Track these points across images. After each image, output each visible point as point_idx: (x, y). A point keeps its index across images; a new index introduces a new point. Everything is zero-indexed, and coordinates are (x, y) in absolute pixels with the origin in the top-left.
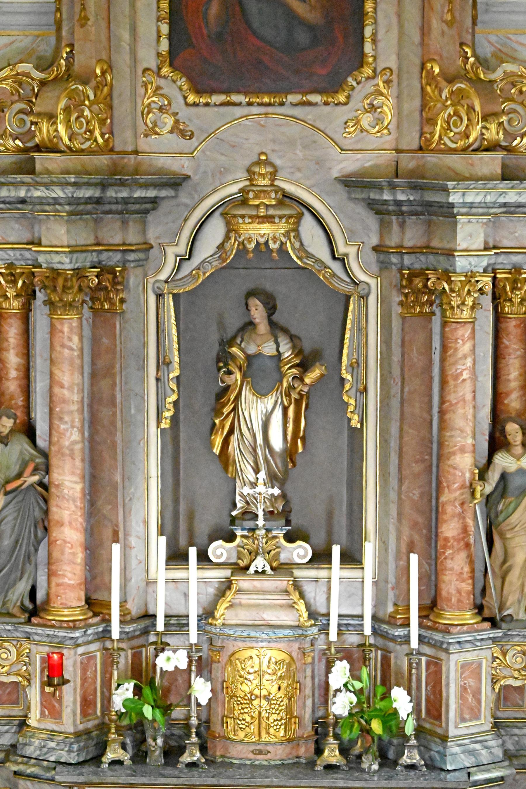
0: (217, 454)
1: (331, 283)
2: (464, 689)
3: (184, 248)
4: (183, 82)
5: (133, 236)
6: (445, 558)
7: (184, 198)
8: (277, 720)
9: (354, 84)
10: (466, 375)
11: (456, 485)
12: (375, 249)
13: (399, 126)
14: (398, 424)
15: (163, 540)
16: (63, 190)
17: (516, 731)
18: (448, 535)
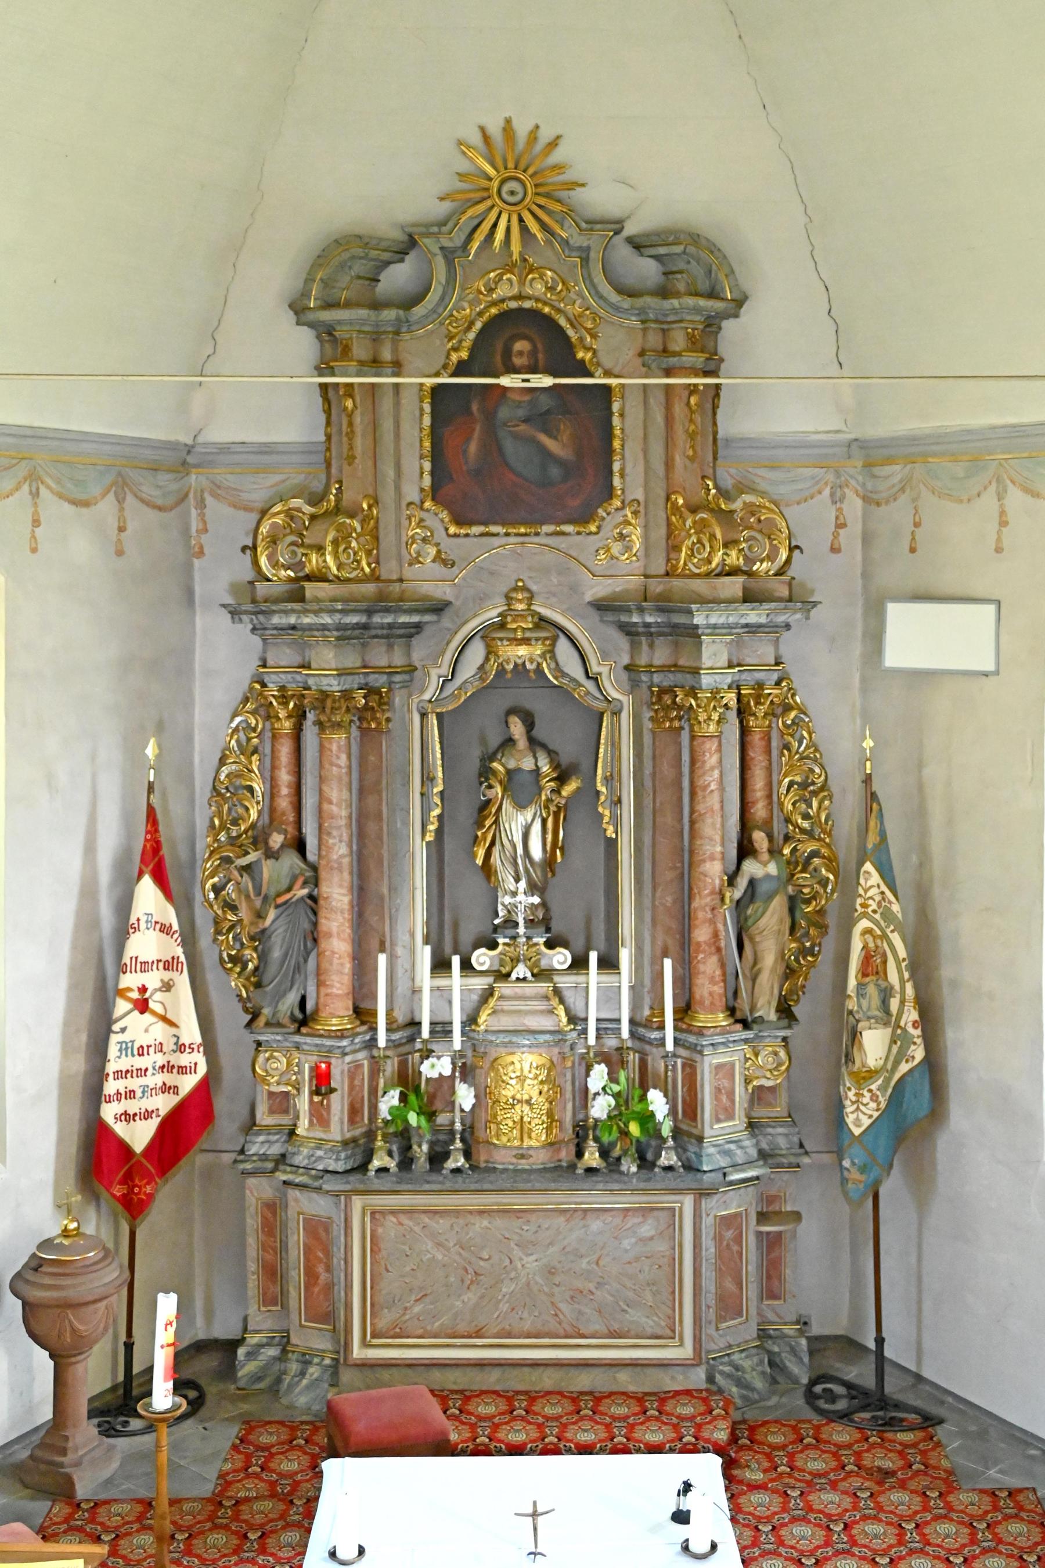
2: (718, 1090)
3: (445, 671)
4: (444, 515)
5: (398, 659)
6: (698, 962)
7: (446, 621)
9: (604, 514)
10: (713, 786)
13: (647, 555)
15: (428, 949)
17: (770, 1130)
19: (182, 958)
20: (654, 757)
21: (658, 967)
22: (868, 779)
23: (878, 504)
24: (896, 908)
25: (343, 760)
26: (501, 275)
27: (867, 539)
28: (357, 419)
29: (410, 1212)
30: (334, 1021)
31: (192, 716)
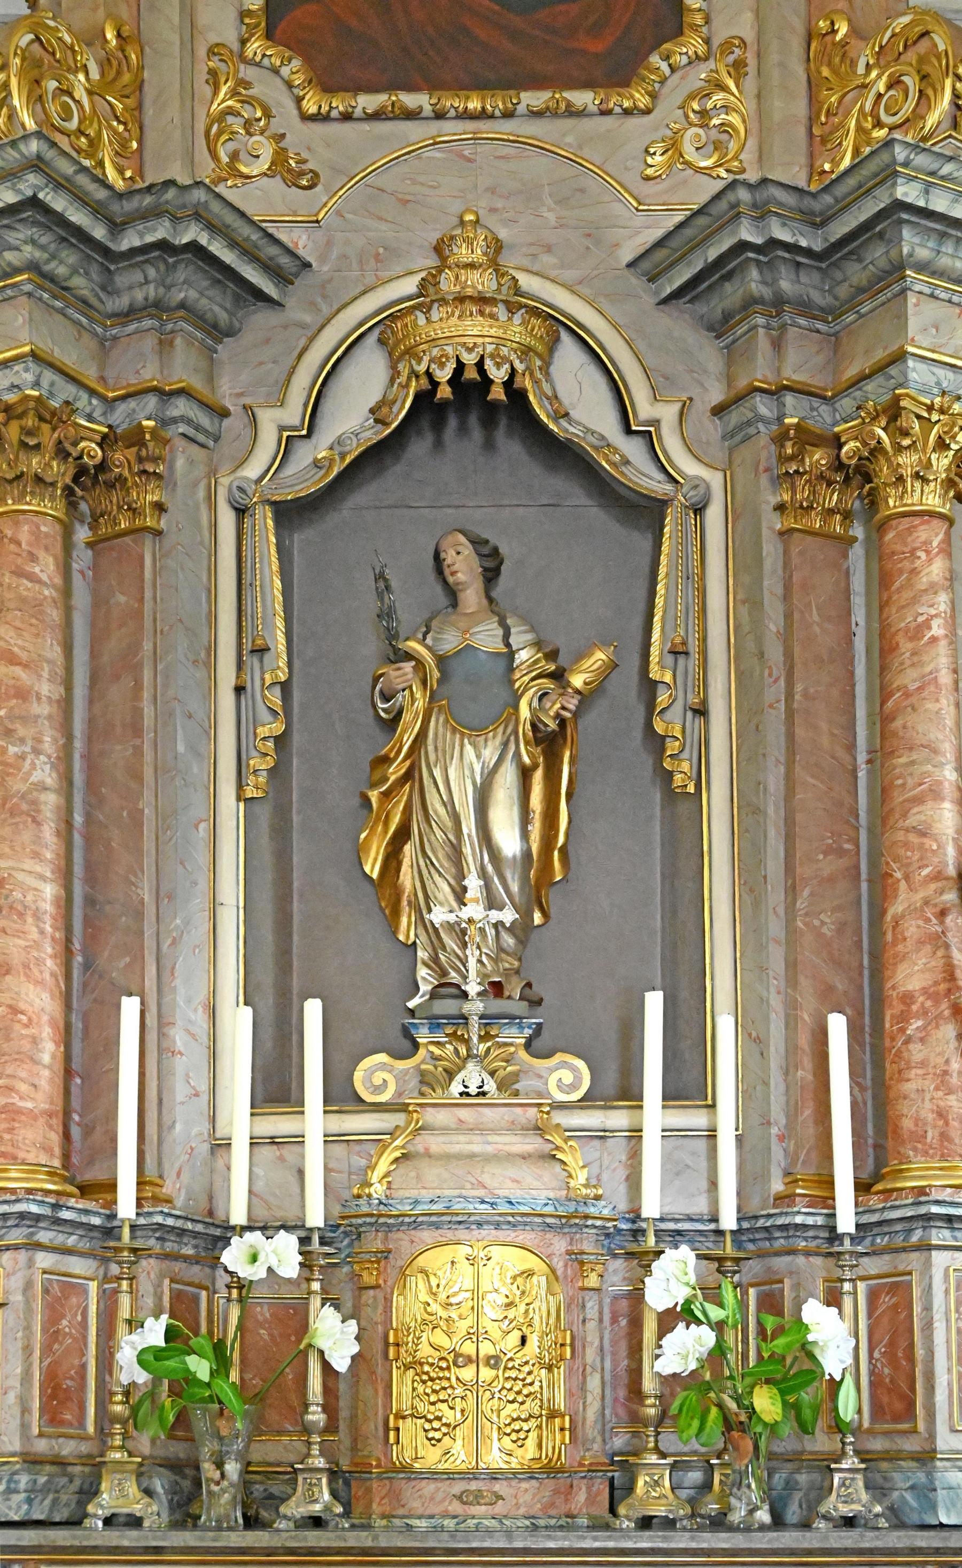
0: (375, 875)
1: (622, 473)
4: (294, 69)
6: (908, 1041)
8: (518, 1419)
9: (664, 66)
10: (937, 629)
11: (925, 872)
14: (782, 769)
16: (13, 188)
18: (910, 987)
20: (787, 596)
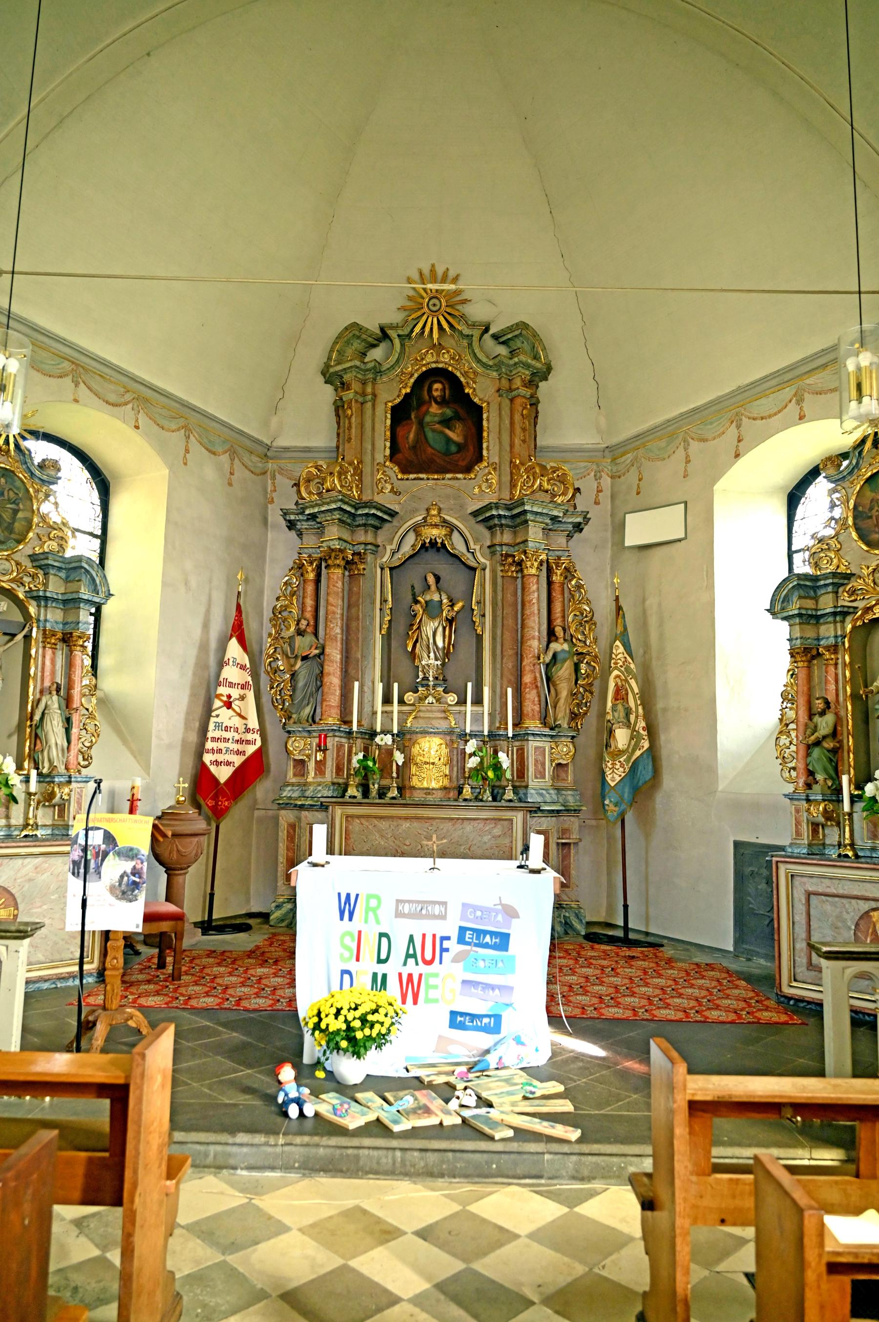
2: (536, 761)
3: (396, 544)
4: (396, 469)
5: (370, 538)
7: (395, 522)
10: (534, 601)
12: (489, 547)
13: (500, 489)
15: (381, 685)
19: (251, 683)
21: (504, 700)
22: (617, 597)
23: (619, 477)
24: (632, 666)
25: (340, 584)
26: (428, 351)
27: (613, 497)
28: (353, 419)
29: (368, 817)
30: (330, 719)
31: (264, 581)
